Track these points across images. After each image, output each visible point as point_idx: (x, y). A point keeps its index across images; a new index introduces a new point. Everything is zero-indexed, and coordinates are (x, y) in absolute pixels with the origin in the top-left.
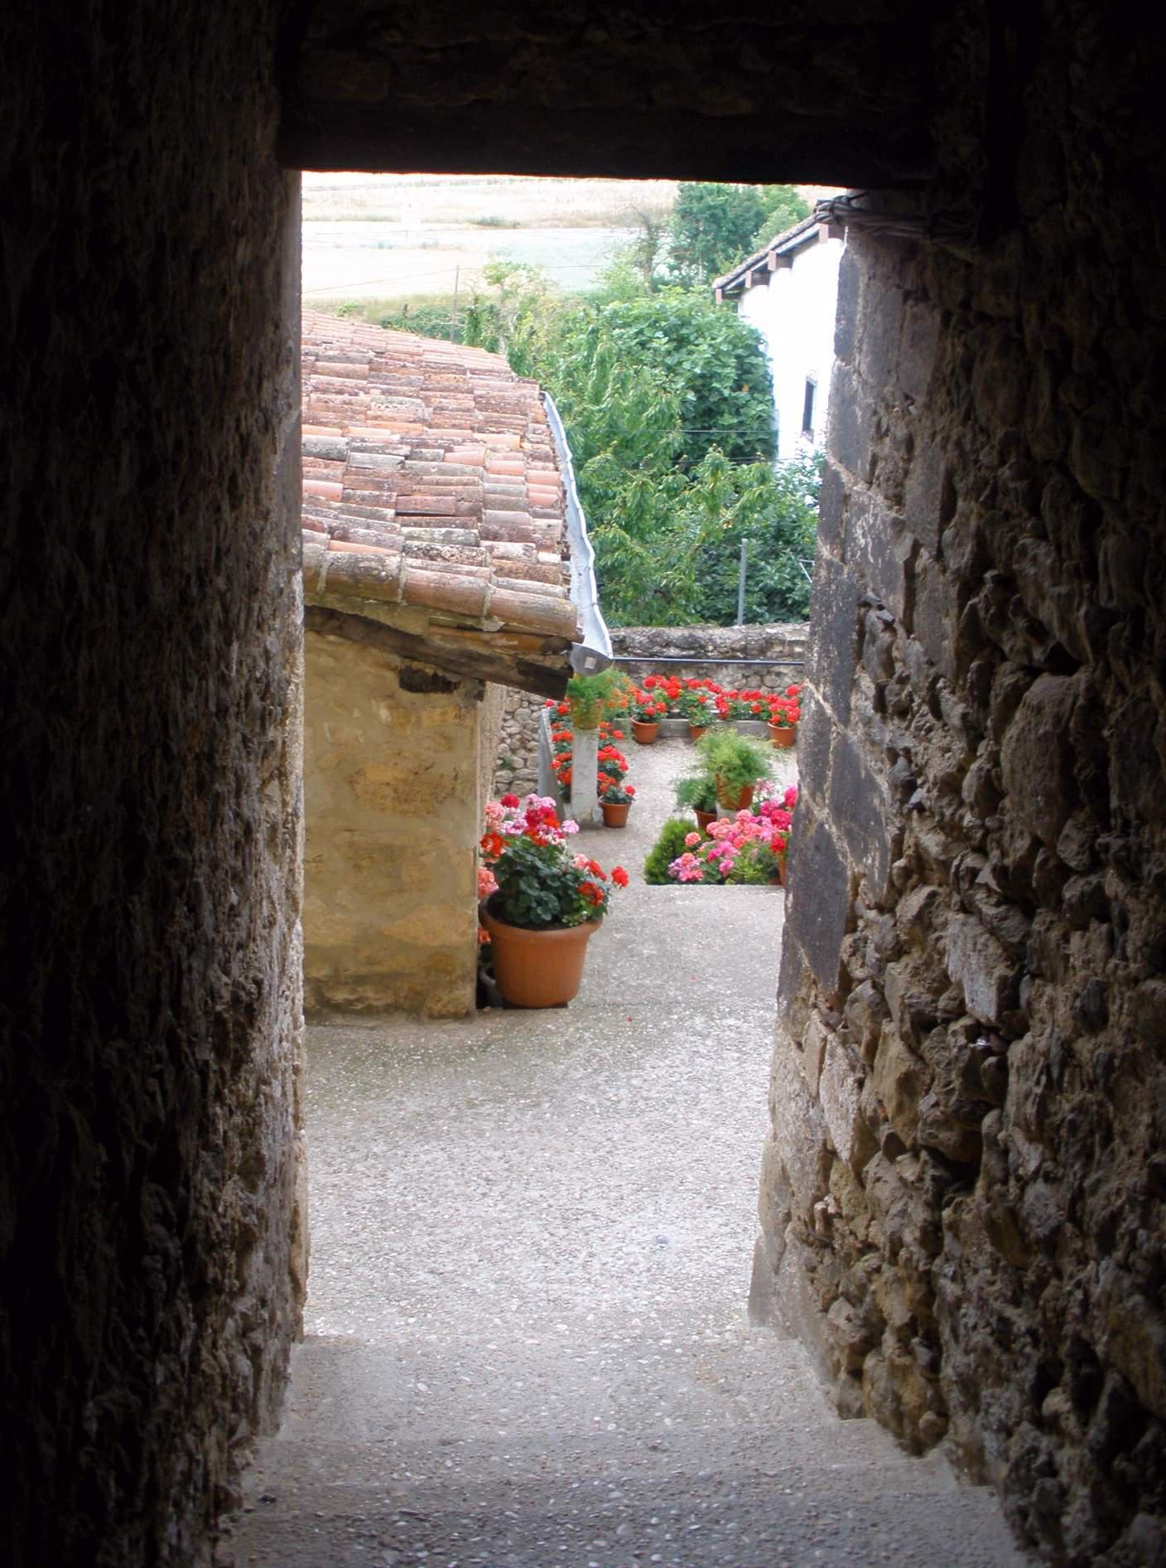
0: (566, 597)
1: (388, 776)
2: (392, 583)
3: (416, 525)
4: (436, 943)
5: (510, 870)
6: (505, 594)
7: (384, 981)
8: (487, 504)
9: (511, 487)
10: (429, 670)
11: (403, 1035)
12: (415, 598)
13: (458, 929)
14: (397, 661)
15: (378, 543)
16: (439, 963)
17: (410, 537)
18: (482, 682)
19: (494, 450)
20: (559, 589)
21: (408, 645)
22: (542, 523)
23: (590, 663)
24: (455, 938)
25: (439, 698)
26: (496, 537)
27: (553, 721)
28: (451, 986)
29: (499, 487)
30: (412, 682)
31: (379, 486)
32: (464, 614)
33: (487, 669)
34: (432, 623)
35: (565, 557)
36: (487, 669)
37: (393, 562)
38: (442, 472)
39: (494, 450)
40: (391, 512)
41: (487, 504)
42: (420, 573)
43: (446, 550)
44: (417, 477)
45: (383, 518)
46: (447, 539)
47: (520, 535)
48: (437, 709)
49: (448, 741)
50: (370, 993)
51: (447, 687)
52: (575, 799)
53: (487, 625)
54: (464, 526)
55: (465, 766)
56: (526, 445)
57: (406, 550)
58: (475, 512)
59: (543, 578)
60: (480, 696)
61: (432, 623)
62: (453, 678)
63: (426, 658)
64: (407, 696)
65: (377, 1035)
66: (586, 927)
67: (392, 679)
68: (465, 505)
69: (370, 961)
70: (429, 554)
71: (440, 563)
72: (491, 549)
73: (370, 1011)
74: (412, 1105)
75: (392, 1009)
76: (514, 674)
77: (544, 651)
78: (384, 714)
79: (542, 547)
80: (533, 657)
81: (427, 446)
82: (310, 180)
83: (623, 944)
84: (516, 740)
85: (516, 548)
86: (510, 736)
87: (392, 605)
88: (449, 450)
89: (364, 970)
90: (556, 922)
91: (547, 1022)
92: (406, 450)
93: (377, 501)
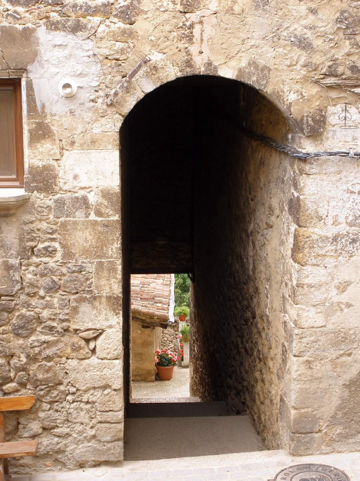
0: (168, 313)
1: (140, 342)
2: (140, 312)
3: (144, 301)
4: (148, 369)
5: (161, 357)
6: (158, 313)
7: (140, 375)
8: (155, 296)
9: (160, 293)
10: (146, 325)
11: (143, 384)
12: (144, 314)
13: (151, 366)
14: (141, 323)
15: (138, 305)
16: (149, 373)
17: (143, 304)
18: (154, 327)
19: (157, 284)
20: (166, 312)
21: (143, 321)
22: (165, 300)
23: (170, 323)
24: (151, 368)
25: (148, 329)
26: (157, 303)
27: (180, 341)
28: (151, 376)
29: (158, 293)
30: (144, 327)
31: (137, 294)
32: (151, 316)
33: (155, 324)
34: (147, 318)
35: (169, 306)
36: (155, 324)
37: (140, 308)
38: (148, 290)
39: (157, 284)
40: (139, 299)
41: (155, 296)
42: (144, 310)
43: (148, 306)
44: (143, 291)
45: (138, 300)
46: (149, 304)
47: (161, 302)
48: (147, 331)
49: (149, 336)
50: (138, 378)
51: (149, 327)
52: (184, 360)
53: (155, 318)
54: (152, 301)
55: (152, 340)
56: (165, 282)
57: (142, 306)
58: (153, 298)
59: (164, 310)
60: (154, 329)
61: (147, 318)
62: (150, 326)
63: (146, 323)
64: (143, 329)
65: (139, 384)
66: (172, 366)
67: (140, 326)
68: (152, 297)
69: (138, 372)
70: (146, 306)
71: (148, 308)
72: (156, 305)
73: (138, 381)
74: (145, 393)
75: (141, 380)
76: (159, 325)
77: (163, 322)
78: (139, 332)
79: (164, 304)
80: (162, 323)
81: (145, 285)
82: (131, 275)
83: (183, 376)
84: (173, 349)
85: (160, 305)
86: (171, 348)
87: (140, 315)
88: (149, 285)
89: (137, 374)
90: (168, 365)
91: (167, 382)
92: (141, 286)
93: (137, 297)
